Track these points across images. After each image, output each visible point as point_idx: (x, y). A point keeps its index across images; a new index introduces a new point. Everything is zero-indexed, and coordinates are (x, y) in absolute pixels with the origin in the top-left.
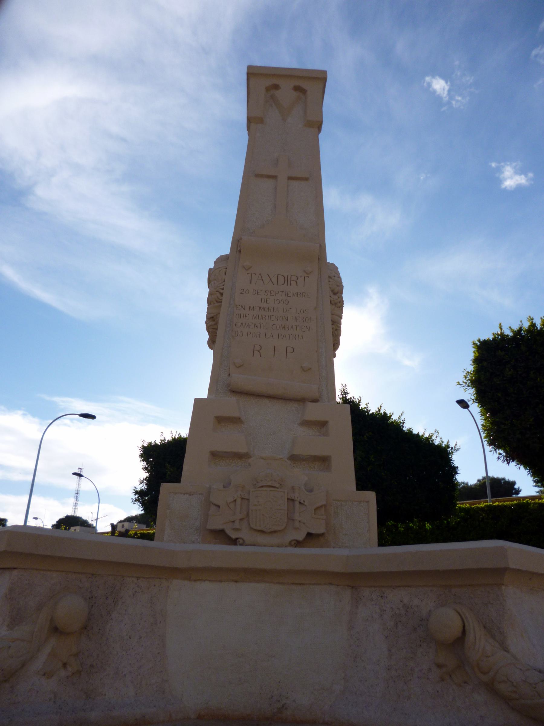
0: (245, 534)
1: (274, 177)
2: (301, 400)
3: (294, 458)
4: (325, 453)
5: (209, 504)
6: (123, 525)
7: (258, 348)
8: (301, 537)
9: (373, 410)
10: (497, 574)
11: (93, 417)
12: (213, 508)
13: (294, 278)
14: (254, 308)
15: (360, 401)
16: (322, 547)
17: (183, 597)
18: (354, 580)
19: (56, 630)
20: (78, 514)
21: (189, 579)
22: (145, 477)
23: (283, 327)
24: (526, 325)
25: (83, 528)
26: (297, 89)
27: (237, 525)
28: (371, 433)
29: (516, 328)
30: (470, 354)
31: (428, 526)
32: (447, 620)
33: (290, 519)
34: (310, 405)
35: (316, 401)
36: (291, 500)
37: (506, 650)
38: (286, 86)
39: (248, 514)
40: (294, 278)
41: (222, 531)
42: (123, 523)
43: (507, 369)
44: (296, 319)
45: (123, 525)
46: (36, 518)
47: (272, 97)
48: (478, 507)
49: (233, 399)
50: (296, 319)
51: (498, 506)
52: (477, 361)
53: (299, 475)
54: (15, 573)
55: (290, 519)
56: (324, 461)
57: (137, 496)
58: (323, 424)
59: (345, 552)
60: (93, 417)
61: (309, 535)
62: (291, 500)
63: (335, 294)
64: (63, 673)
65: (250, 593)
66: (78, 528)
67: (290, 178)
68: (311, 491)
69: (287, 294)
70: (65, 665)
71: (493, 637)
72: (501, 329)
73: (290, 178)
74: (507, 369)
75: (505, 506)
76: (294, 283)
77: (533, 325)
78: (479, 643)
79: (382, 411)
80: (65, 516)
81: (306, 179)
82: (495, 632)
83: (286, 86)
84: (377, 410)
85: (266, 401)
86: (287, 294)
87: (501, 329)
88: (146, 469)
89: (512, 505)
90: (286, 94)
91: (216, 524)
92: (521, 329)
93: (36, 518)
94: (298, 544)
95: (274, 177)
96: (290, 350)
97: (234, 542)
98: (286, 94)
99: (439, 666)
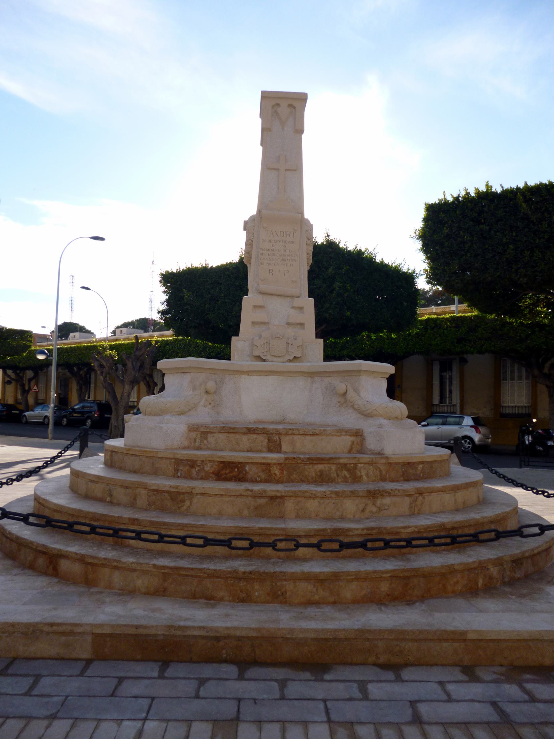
0: (269, 357)
1: (278, 169)
2: (292, 297)
3: (288, 324)
4: (302, 322)
5: (253, 346)
6: (121, 331)
7: (271, 271)
8: (291, 358)
9: (351, 248)
10: (358, 372)
11: (102, 239)
12: (255, 347)
13: (288, 233)
14: (269, 250)
15: (339, 243)
16: (300, 362)
17: (246, 381)
18: (312, 374)
19: (207, 392)
20: (74, 321)
21: (248, 375)
22: (165, 299)
23: (283, 260)
24: (463, 193)
25: (82, 334)
26: (290, 106)
27: (265, 354)
28: (348, 267)
29: (455, 195)
30: (422, 214)
31: (393, 336)
32: (341, 387)
33: (287, 351)
34: (296, 299)
35: (298, 297)
36: (287, 343)
37: (360, 396)
38: (284, 104)
39: (269, 349)
40: (288, 233)
41: (259, 356)
42: (121, 329)
43: (445, 228)
44: (289, 255)
45: (121, 331)
46: (44, 327)
47: (276, 112)
48: (443, 318)
49: (260, 296)
50: (289, 255)
51: (461, 316)
52: (426, 220)
53: (291, 332)
54: (192, 374)
55: (287, 351)
56: (302, 325)
57: (160, 314)
58: (302, 308)
59: (309, 364)
60: (102, 239)
61: (295, 357)
62: (287, 343)
63: (309, 240)
64: (210, 406)
65: (271, 380)
66: (77, 334)
67: (286, 170)
68: (296, 339)
69: (285, 242)
70: (210, 404)
71: (356, 392)
72: (445, 196)
73: (286, 170)
74: (445, 228)
75: (466, 317)
76: (288, 236)
77: (468, 194)
78: (351, 394)
79: (358, 248)
80: (63, 322)
81: (295, 170)
82: (356, 391)
83: (284, 104)
84: (354, 247)
85: (276, 297)
86: (285, 242)
87: (445, 196)
88: (165, 292)
89: (472, 316)
90: (284, 110)
91: (256, 353)
92: (459, 196)
93: (44, 327)
94: (290, 361)
95: (278, 169)
96: (287, 272)
97: (264, 361)
98: (284, 110)
99: (339, 402)
